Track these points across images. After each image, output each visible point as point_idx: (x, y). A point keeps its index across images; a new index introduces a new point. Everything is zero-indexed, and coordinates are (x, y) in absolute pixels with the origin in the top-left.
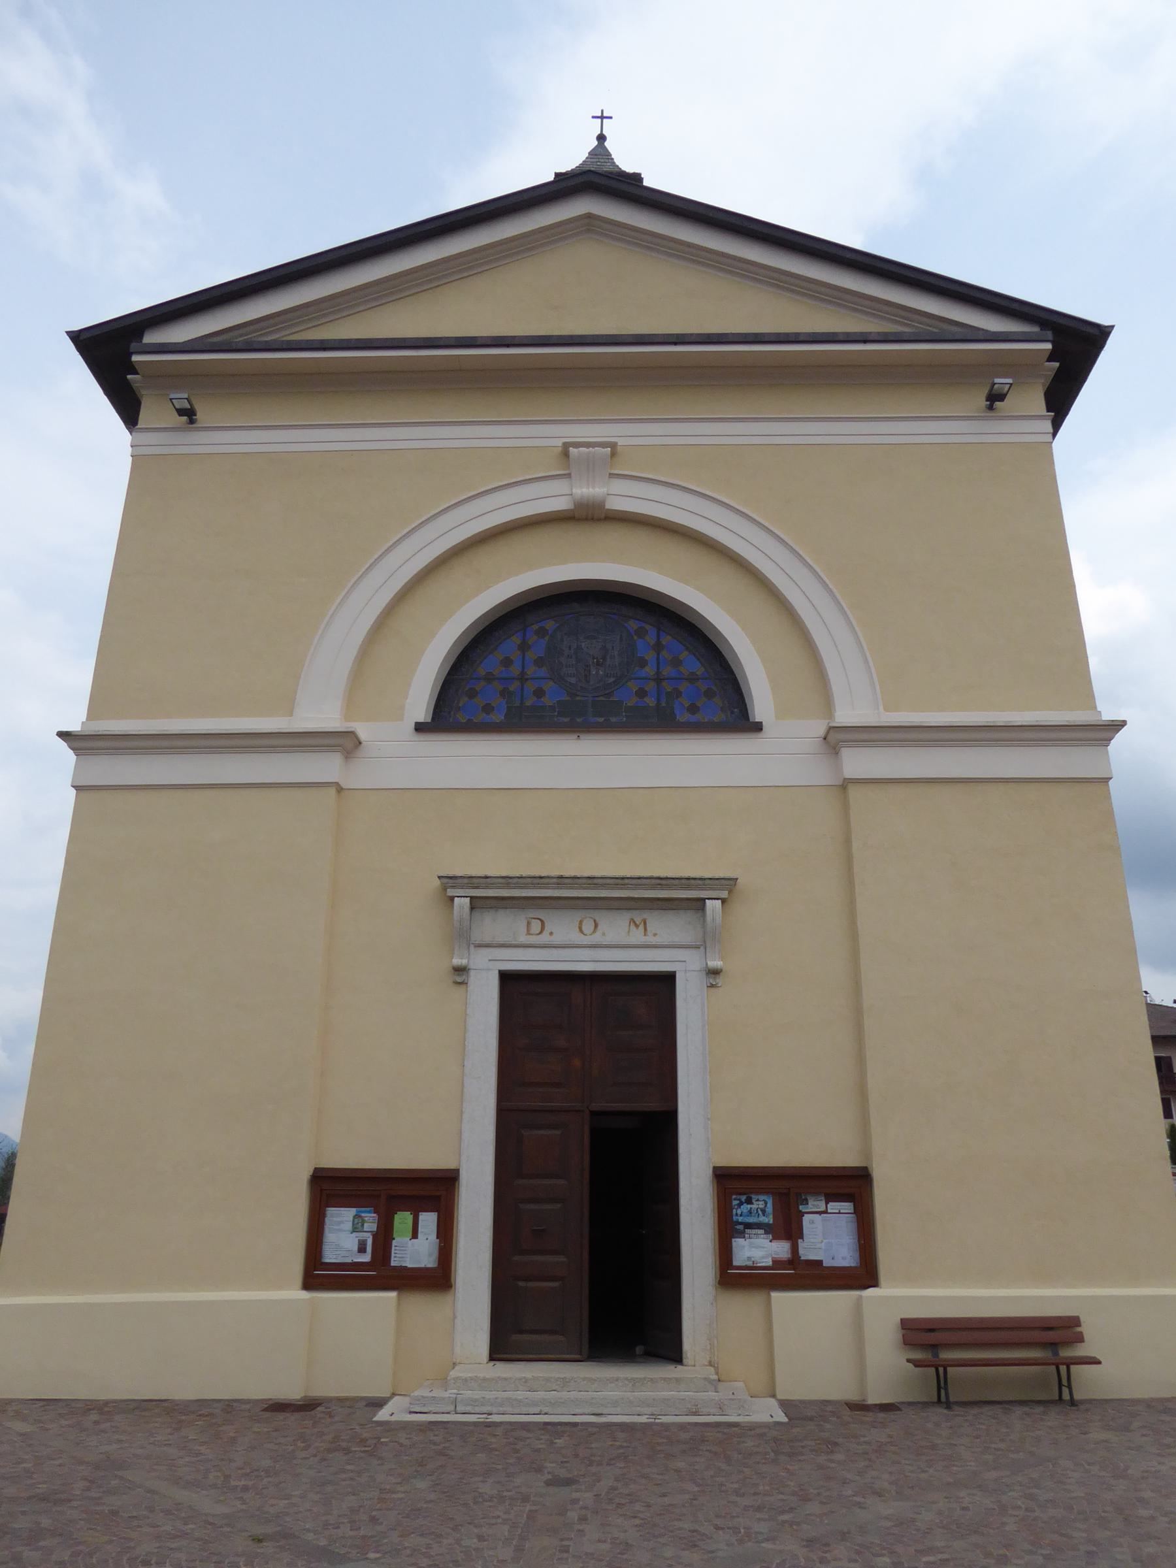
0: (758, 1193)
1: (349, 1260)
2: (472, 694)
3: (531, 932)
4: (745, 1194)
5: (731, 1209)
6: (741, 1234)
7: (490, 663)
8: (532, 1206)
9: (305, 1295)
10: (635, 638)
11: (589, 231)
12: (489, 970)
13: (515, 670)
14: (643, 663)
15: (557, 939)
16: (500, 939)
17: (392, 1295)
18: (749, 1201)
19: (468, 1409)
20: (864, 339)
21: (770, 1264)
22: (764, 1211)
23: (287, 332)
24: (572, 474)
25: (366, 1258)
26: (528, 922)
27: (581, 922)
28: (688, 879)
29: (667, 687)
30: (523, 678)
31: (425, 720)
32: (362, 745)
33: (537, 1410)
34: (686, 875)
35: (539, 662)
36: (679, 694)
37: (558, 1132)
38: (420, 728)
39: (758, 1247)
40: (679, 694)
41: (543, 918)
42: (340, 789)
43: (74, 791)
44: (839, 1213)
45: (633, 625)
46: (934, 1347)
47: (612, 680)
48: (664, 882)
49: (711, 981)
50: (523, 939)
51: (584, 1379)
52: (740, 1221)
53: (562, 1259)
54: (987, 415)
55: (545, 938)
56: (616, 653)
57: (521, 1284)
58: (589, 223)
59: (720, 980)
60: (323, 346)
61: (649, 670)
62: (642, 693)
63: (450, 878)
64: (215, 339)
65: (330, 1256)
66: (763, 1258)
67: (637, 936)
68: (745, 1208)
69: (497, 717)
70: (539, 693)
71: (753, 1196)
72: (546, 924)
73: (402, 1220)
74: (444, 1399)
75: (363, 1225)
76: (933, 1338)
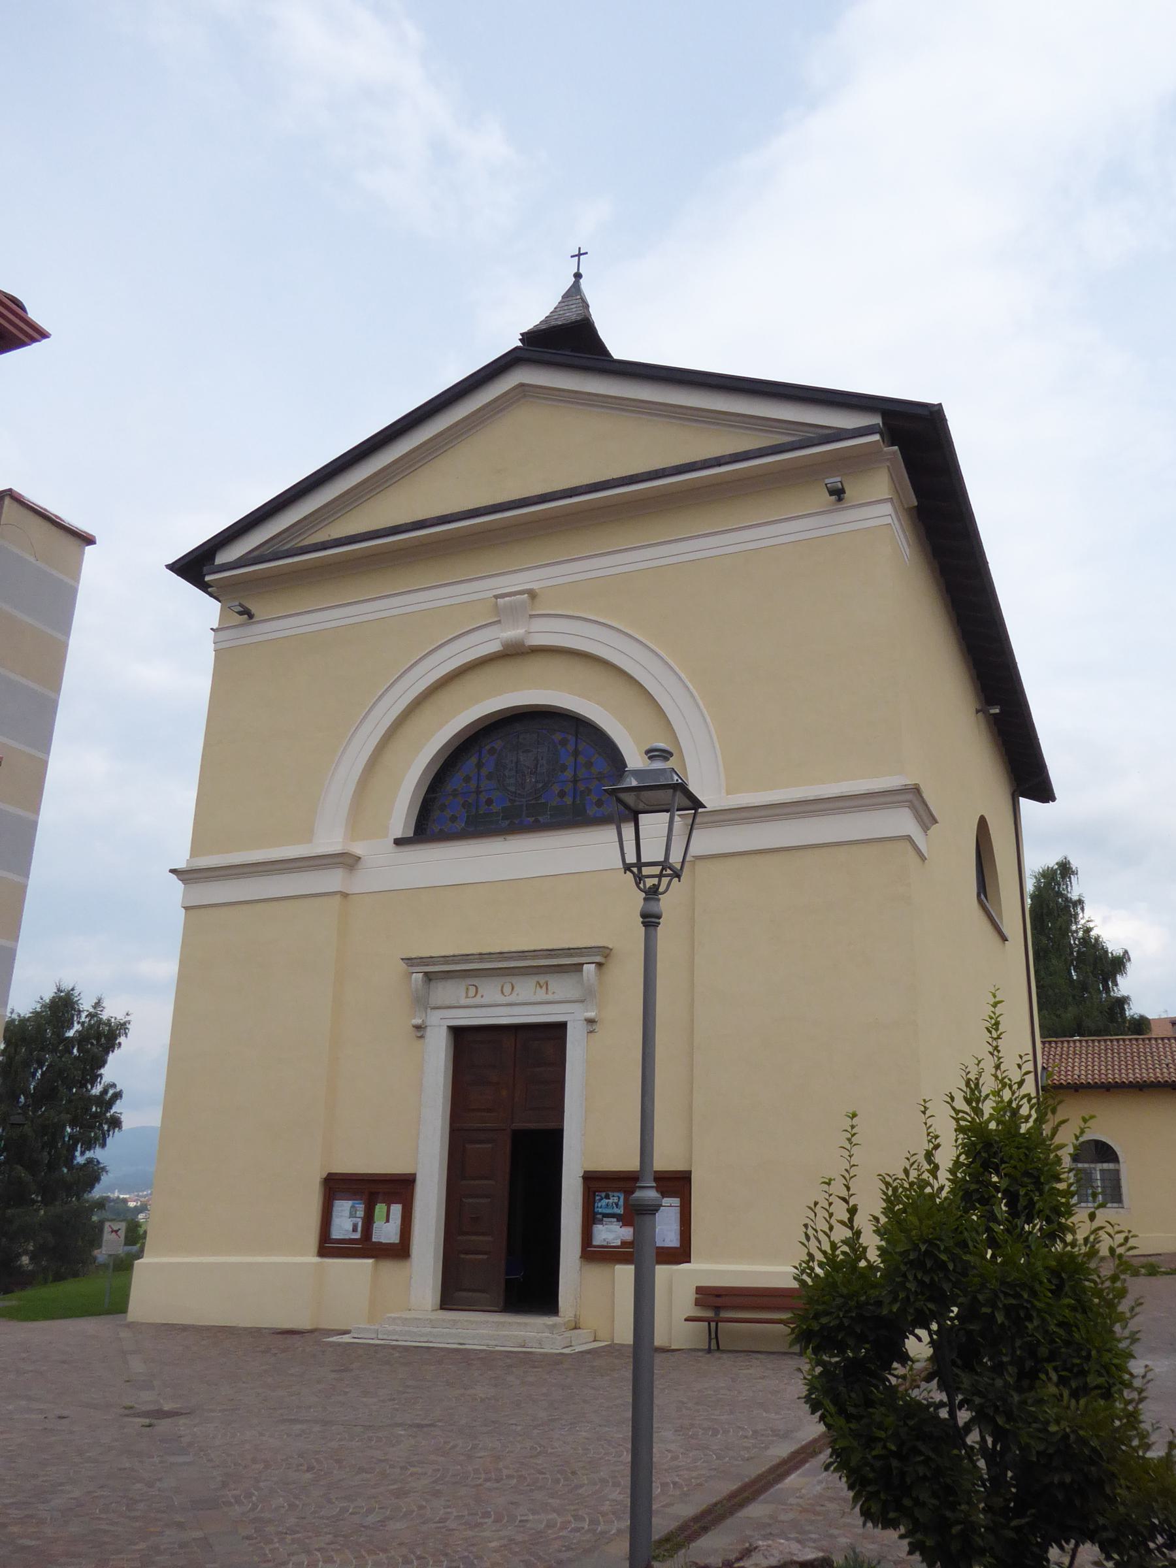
0: (613, 1191)
1: (347, 1237)
2: (443, 808)
3: (469, 996)
4: (604, 1191)
5: (594, 1202)
6: (601, 1222)
7: (455, 782)
8: (470, 1200)
9: (318, 1260)
10: (559, 747)
11: (525, 396)
12: (440, 1026)
13: (473, 785)
14: (564, 768)
15: (485, 1001)
16: (447, 1003)
17: (370, 1261)
18: (607, 1197)
19: (385, 1337)
20: (718, 462)
21: (619, 1244)
22: (617, 1205)
23: (300, 539)
24: (502, 621)
25: (357, 1236)
26: (467, 989)
27: (502, 987)
28: (569, 949)
29: (581, 787)
30: (478, 792)
31: (403, 832)
32: (362, 860)
33: (426, 1340)
34: (567, 946)
35: (490, 777)
36: (589, 791)
37: (490, 1145)
38: (399, 842)
39: (610, 1231)
40: (589, 791)
41: (477, 985)
42: (345, 895)
43: (183, 910)
44: (671, 1206)
45: (558, 737)
46: (717, 1309)
47: (540, 785)
48: (553, 953)
49: (589, 1027)
50: (463, 1002)
51: (467, 1321)
52: (600, 1211)
53: (490, 1238)
54: (834, 507)
55: (478, 1000)
56: (545, 762)
57: (462, 1256)
58: (523, 390)
59: (595, 1027)
60: (324, 546)
61: (569, 774)
62: (562, 794)
63: (408, 959)
64: (256, 553)
65: (336, 1234)
66: (614, 1240)
67: (541, 995)
68: (605, 1201)
69: (460, 825)
70: (489, 802)
71: (610, 1193)
72: (479, 990)
73: (380, 1209)
74: (371, 1329)
75: (356, 1213)
76: (719, 1302)
